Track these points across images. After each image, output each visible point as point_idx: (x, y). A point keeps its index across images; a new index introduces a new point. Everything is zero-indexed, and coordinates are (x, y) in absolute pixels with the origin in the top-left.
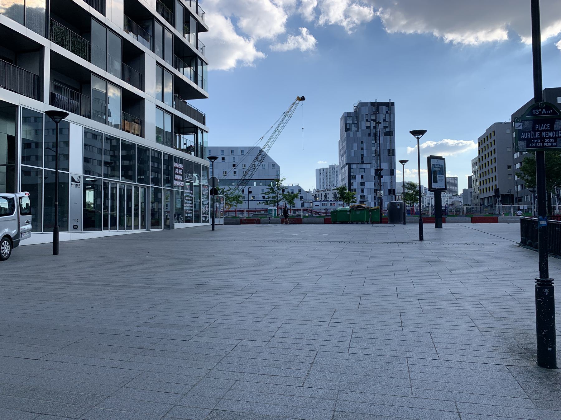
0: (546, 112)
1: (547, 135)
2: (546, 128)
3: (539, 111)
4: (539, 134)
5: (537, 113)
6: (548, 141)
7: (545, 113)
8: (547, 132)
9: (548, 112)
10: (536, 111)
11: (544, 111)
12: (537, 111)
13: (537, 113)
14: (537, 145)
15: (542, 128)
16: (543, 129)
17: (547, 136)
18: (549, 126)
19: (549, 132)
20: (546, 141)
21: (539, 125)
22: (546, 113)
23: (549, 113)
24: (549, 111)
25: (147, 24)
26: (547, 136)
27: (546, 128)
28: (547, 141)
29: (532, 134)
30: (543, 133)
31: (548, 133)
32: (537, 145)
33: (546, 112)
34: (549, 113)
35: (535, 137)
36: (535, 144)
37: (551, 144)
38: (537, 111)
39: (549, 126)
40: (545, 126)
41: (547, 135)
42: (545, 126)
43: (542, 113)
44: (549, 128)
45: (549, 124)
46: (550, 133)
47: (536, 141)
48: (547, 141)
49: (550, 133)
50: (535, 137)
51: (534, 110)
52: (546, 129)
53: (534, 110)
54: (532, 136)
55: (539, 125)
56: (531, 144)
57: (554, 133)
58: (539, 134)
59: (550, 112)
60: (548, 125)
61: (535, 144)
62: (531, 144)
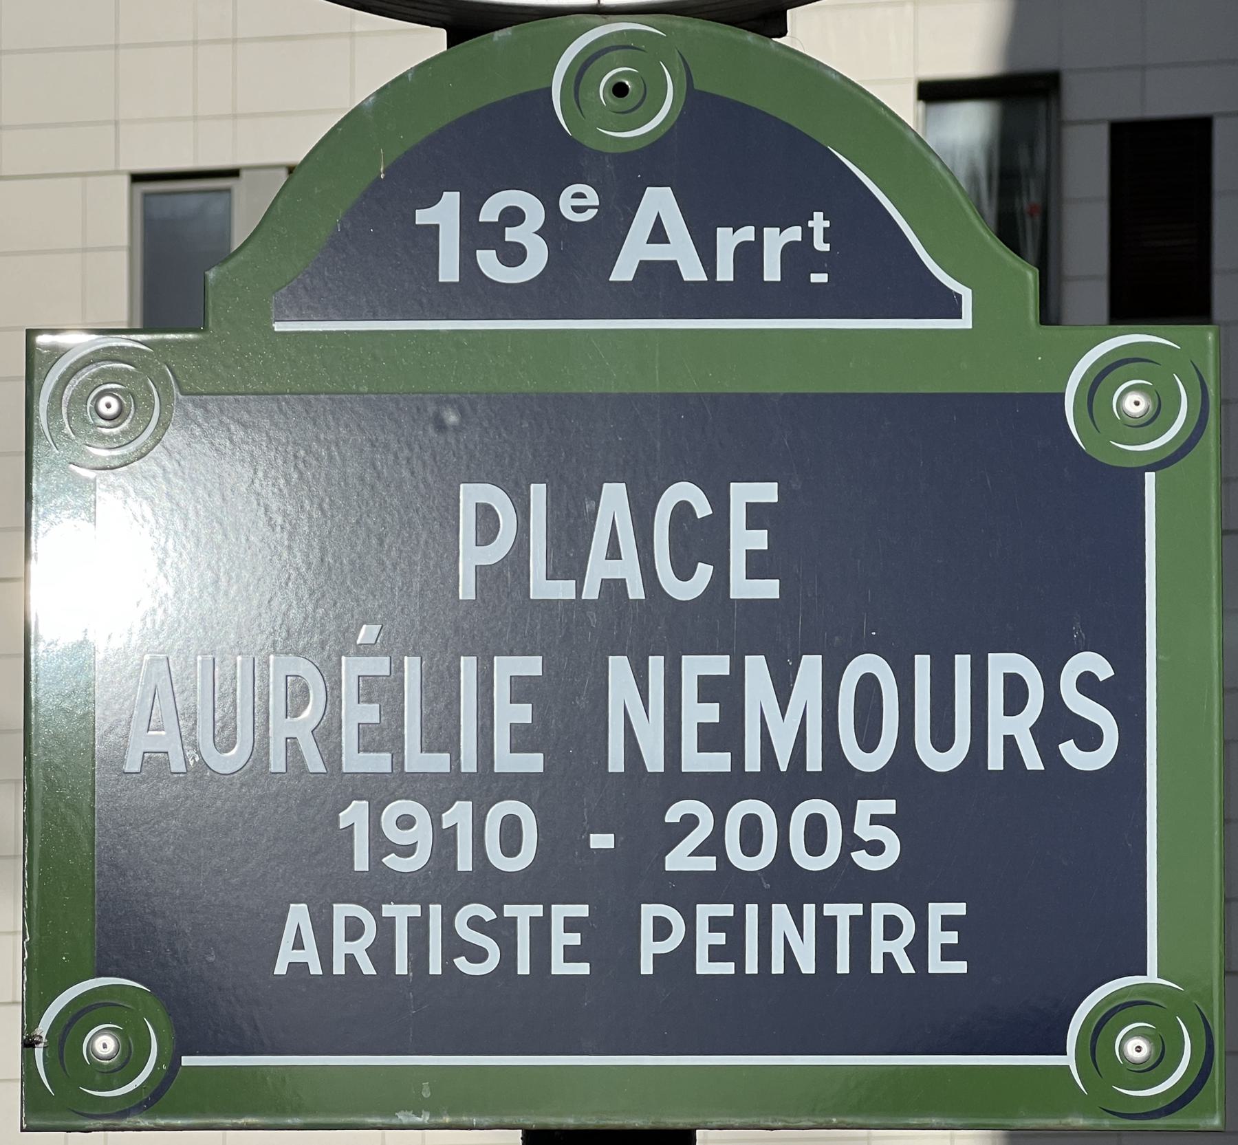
0: (708, 256)
1: (710, 739)
2: (684, 572)
3: (554, 228)
4: (522, 690)
5: (513, 255)
6: (751, 841)
7: (671, 267)
8: (719, 665)
9: (749, 256)
10: (490, 212)
11: (658, 235)
12: (514, 216)
13: (513, 255)
14: (454, 946)
15: (599, 568)
16: (614, 588)
17: (728, 968)
18: (757, 515)
19: (757, 668)
20: (680, 859)
21: (538, 493)
22: (693, 271)
23: (772, 272)
24: (775, 240)
25: (423, 217)
26: (728, 968)
27: (684, 572)
28: (714, 845)
29: (369, 689)
30: (619, 668)
31: (733, 927)
32: (454, 946)
33: (708, 256)
34: (772, 272)
35: (564, 590)
36: (418, 928)
37: (826, 928)
38: (514, 216)
39: (757, 515)
40: (683, 510)
41: (710, 739)
42: (683, 510)
43: (624, 271)
44: (758, 566)
45: (767, 492)
46: (783, 689)
47: (445, 840)
48: (714, 845)
49: (783, 689)
50: (564, 590)
51: (451, 201)
52: (688, 590)
53: (451, 201)
54: (370, 740)
55: (538, 493)
56: (299, 915)
57: (868, 686)
58: (522, 690)
59: (789, 251)
60: (743, 494)
61: (418, 928)
62: (299, 915)
